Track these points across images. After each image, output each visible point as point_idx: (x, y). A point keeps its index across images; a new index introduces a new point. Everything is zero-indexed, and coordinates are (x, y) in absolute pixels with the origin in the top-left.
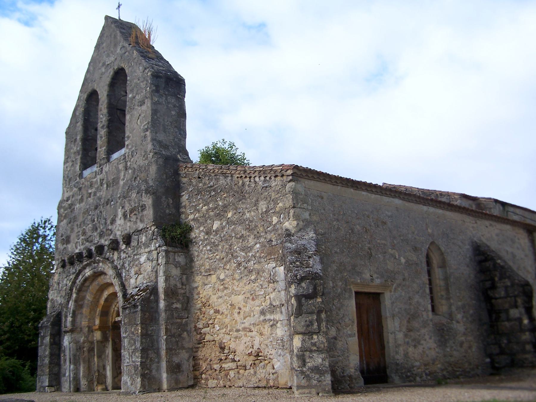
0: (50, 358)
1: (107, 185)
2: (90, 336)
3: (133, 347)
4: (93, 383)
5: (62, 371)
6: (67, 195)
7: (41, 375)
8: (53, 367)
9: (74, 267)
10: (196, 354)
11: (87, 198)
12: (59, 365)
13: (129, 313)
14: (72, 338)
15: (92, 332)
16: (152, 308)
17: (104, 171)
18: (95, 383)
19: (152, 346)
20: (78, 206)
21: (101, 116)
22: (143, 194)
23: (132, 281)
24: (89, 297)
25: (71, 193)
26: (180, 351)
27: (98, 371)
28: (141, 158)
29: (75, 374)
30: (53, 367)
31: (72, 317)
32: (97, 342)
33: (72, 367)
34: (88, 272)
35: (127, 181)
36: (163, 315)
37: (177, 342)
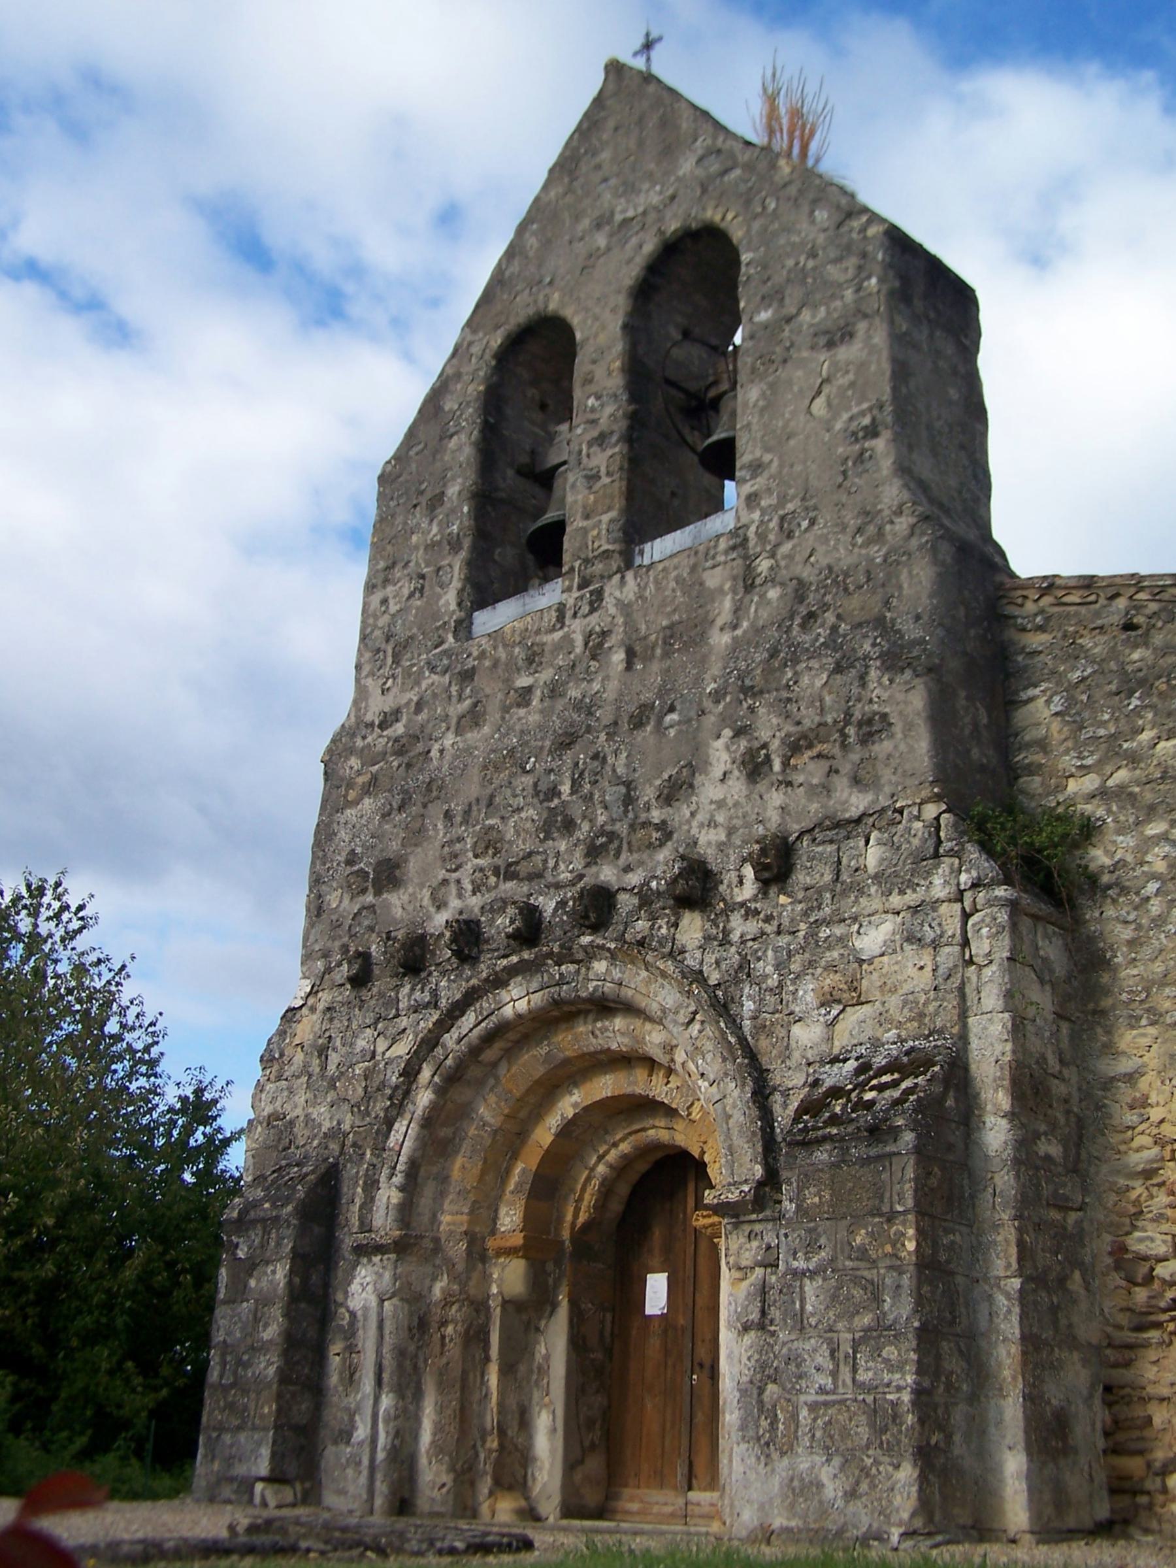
0: (286, 1354)
1: (631, 654)
2: (475, 1276)
3: (866, 1320)
4: (472, 1484)
5: (333, 1416)
6: (377, 705)
7: (221, 1429)
8: (294, 1395)
9: (424, 982)
10: (1126, 1375)
11: (506, 709)
12: (316, 1389)
13: (835, 1166)
14: (395, 1278)
15: (484, 1258)
16: (950, 1147)
17: (609, 602)
18: (485, 1485)
19: (952, 1323)
20: (449, 740)
21: (591, 402)
22: (873, 674)
23: (807, 1035)
24: (489, 1111)
25: (413, 696)
26: (1065, 1355)
27: (502, 1432)
28: (846, 538)
29: (397, 1434)
30: (294, 1395)
31: (402, 1189)
32: (506, 1303)
33: (386, 1401)
34: (517, 1000)
35: (758, 630)
36: (1004, 1180)
37: (1054, 1310)
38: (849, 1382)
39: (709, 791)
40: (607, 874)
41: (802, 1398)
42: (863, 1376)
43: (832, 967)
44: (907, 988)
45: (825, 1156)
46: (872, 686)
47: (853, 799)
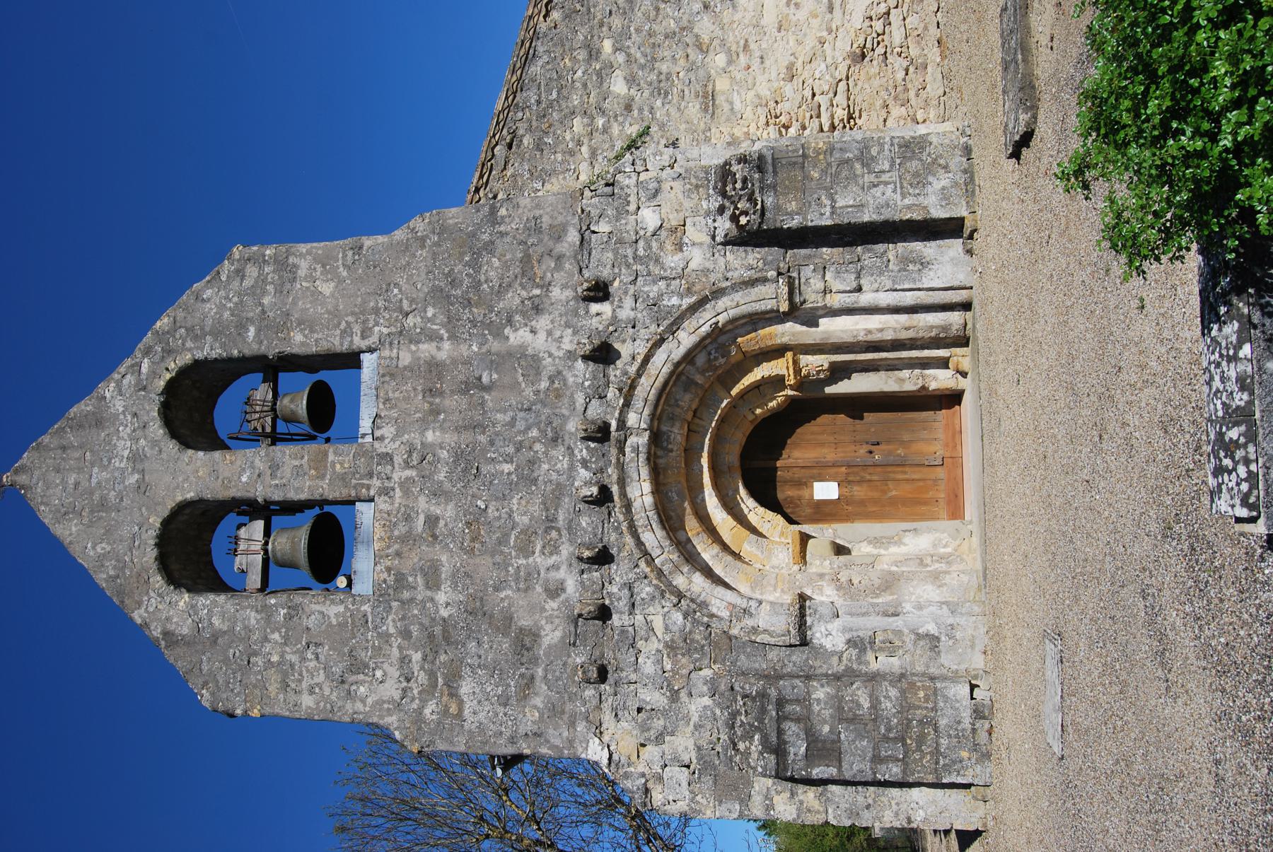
3: (858, 166)
38: (888, 175)
39: (539, 343)
40: (573, 426)
41: (899, 203)
42: (886, 166)
43: (661, 248)
44: (680, 196)
45: (770, 199)
46: (509, 229)
47: (569, 239)
